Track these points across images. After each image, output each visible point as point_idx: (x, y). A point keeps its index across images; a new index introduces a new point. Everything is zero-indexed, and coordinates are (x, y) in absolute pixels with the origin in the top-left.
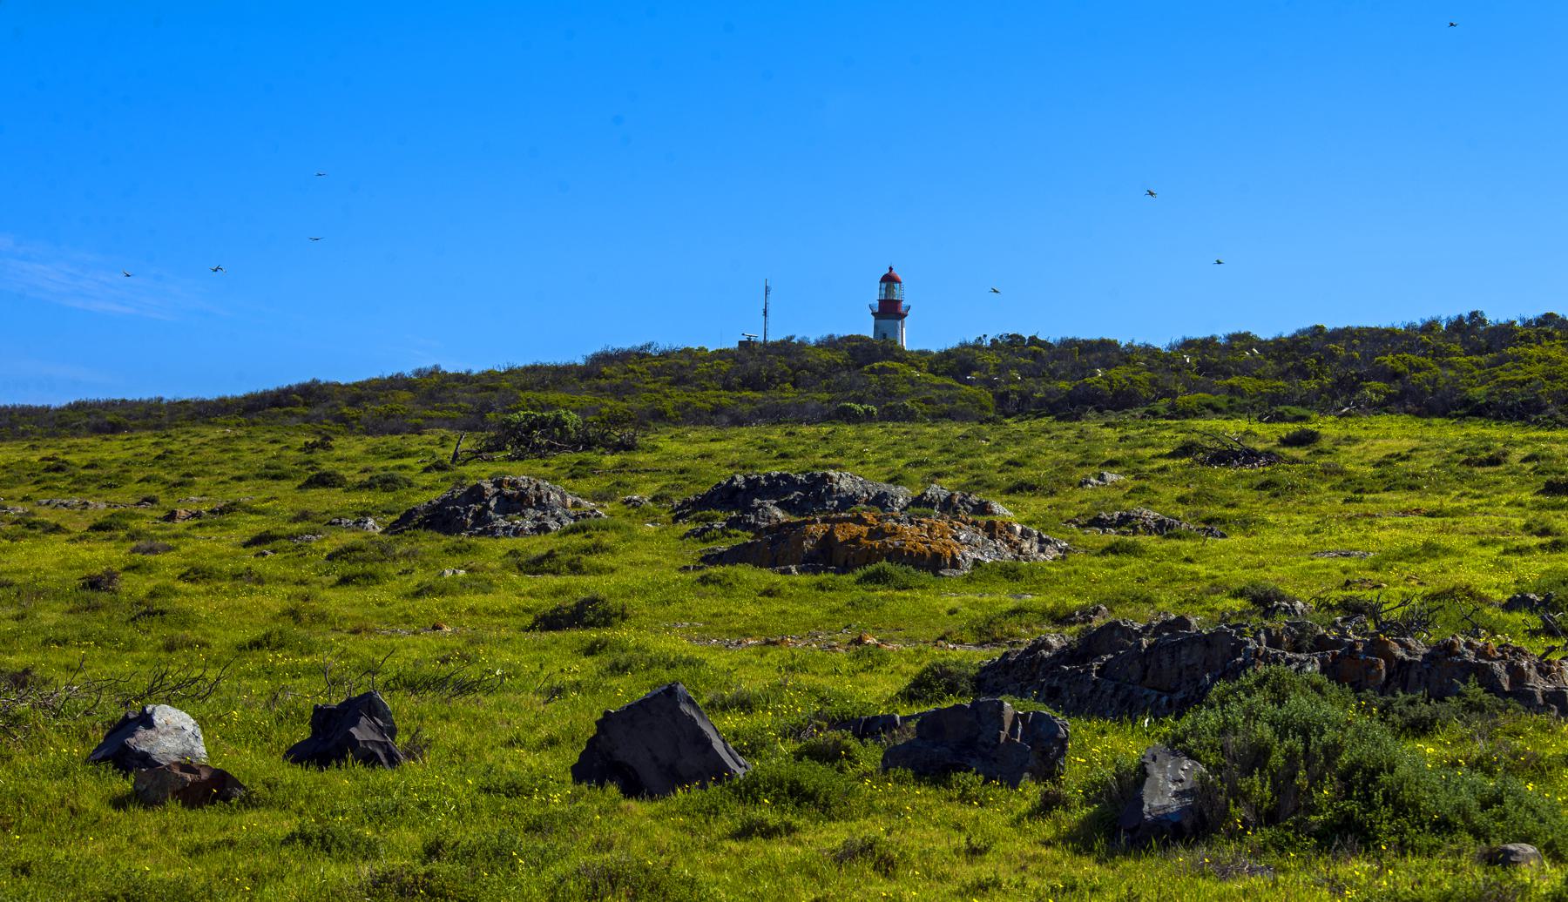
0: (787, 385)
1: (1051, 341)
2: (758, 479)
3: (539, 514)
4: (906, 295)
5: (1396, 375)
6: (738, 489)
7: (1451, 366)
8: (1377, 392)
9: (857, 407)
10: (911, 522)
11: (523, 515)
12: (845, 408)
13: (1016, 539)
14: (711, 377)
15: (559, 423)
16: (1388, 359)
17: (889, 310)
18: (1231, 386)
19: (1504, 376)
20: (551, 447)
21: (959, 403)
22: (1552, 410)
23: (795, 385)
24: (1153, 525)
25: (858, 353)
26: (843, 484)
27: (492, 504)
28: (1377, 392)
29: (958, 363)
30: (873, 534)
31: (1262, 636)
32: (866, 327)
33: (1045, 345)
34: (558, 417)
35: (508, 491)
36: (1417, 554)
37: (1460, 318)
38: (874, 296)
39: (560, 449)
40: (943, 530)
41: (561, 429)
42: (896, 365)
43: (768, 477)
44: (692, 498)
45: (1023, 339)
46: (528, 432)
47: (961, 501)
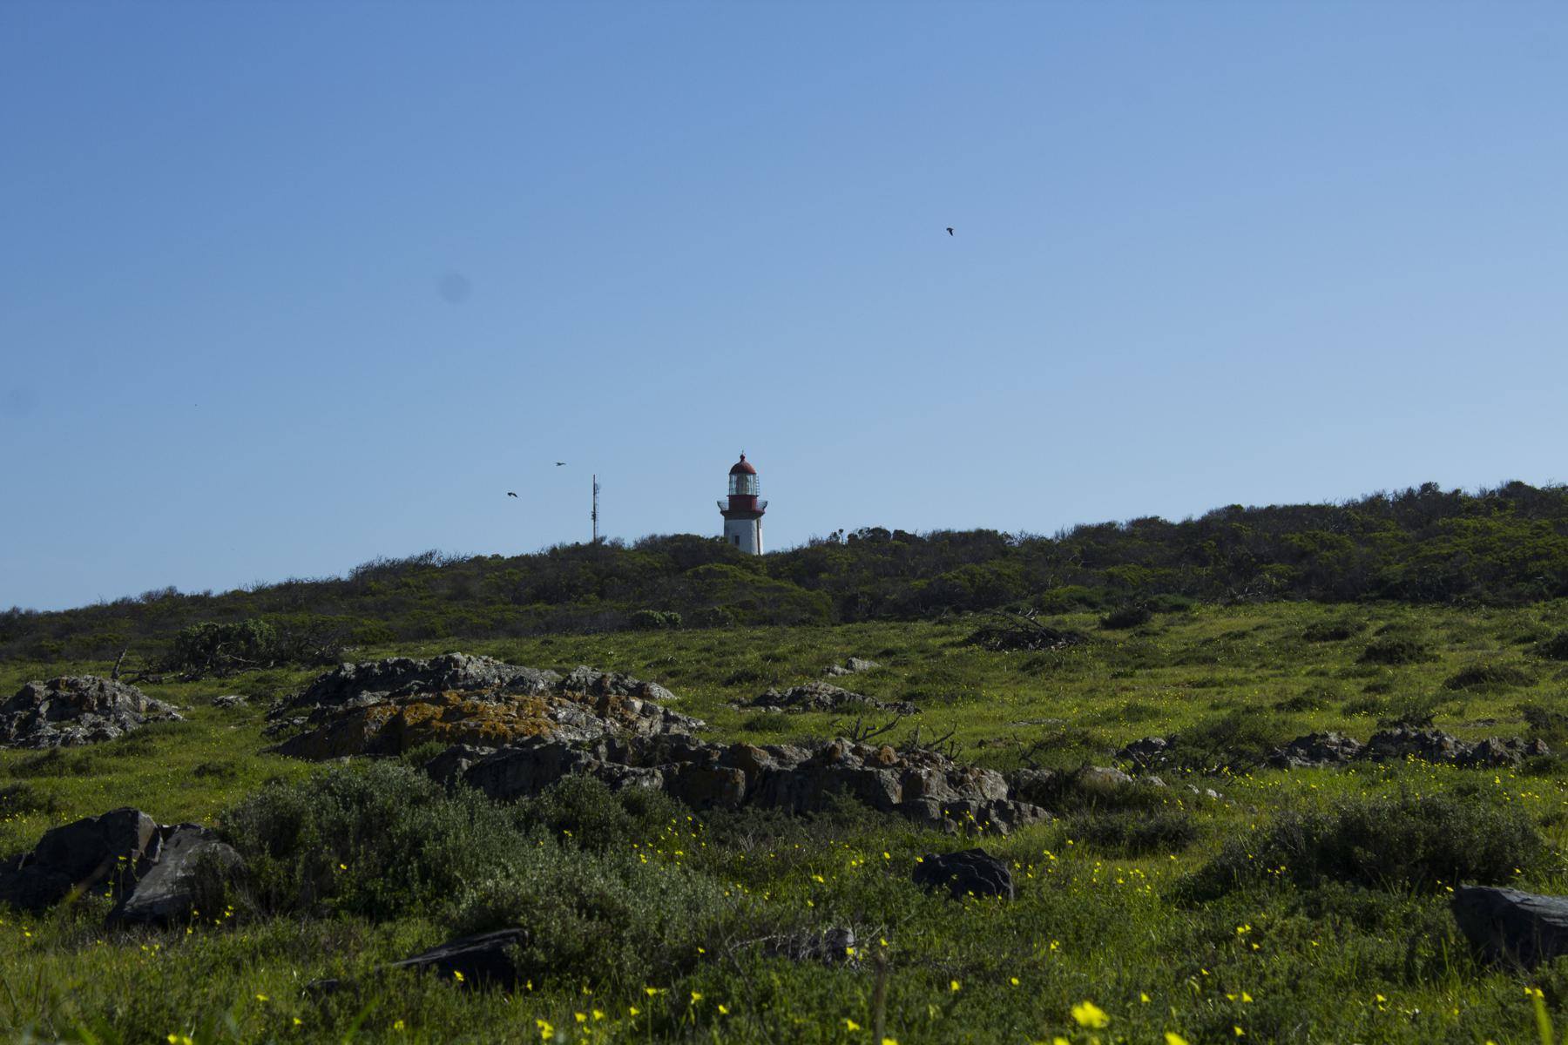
0: (592, 596)
1: (919, 534)
2: (371, 667)
3: (101, 719)
4: (763, 488)
5: (1303, 555)
6: (346, 680)
7: (1371, 542)
8: (1279, 576)
9: (657, 615)
10: (498, 700)
11: (78, 722)
12: (642, 616)
13: (633, 717)
14: (500, 589)
15: (247, 636)
16: (1295, 539)
17: (742, 508)
18: (1111, 576)
19: (1427, 550)
20: (236, 664)
21: (785, 606)
22: (1478, 587)
23: (602, 595)
24: (829, 700)
25: (680, 552)
26: (471, 669)
27: (43, 709)
28: (1279, 576)
29: (808, 564)
30: (447, 717)
31: (602, 749)
32: (711, 526)
33: (912, 539)
34: (244, 627)
35: (64, 693)
36: (1116, 718)
37: (1410, 491)
38: (722, 490)
39: (246, 665)
40: (537, 708)
41: (248, 641)
42: (726, 567)
43: (384, 665)
44: (296, 695)
45: (886, 533)
46: (210, 648)
47: (613, 684)
